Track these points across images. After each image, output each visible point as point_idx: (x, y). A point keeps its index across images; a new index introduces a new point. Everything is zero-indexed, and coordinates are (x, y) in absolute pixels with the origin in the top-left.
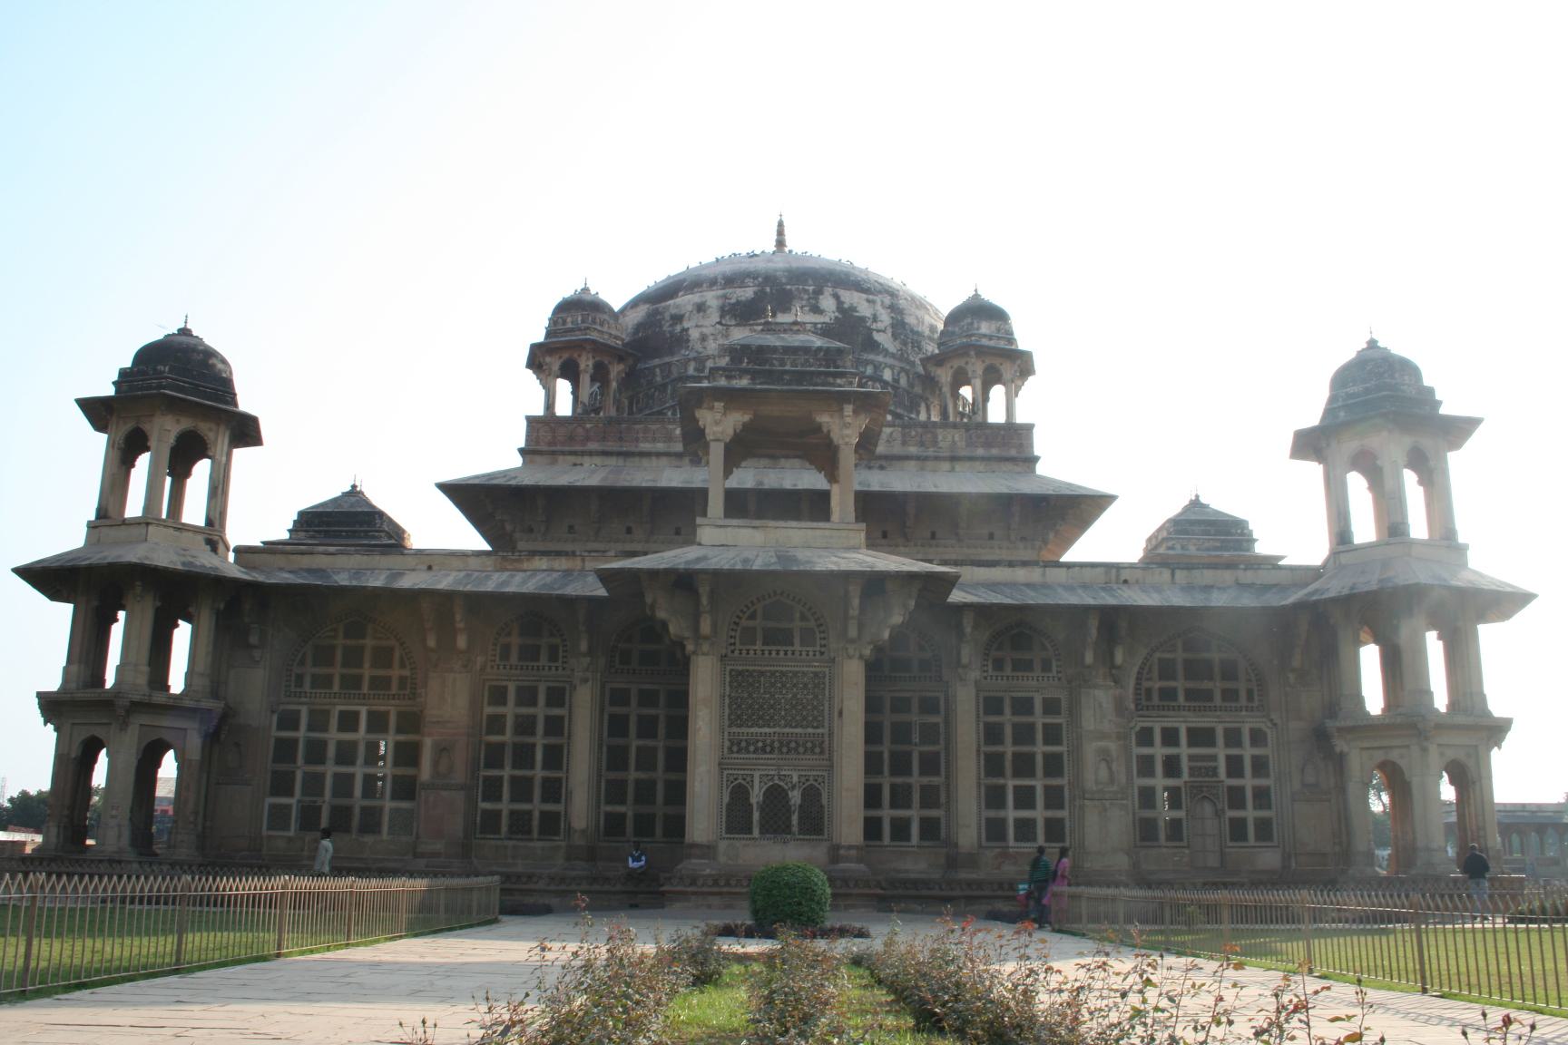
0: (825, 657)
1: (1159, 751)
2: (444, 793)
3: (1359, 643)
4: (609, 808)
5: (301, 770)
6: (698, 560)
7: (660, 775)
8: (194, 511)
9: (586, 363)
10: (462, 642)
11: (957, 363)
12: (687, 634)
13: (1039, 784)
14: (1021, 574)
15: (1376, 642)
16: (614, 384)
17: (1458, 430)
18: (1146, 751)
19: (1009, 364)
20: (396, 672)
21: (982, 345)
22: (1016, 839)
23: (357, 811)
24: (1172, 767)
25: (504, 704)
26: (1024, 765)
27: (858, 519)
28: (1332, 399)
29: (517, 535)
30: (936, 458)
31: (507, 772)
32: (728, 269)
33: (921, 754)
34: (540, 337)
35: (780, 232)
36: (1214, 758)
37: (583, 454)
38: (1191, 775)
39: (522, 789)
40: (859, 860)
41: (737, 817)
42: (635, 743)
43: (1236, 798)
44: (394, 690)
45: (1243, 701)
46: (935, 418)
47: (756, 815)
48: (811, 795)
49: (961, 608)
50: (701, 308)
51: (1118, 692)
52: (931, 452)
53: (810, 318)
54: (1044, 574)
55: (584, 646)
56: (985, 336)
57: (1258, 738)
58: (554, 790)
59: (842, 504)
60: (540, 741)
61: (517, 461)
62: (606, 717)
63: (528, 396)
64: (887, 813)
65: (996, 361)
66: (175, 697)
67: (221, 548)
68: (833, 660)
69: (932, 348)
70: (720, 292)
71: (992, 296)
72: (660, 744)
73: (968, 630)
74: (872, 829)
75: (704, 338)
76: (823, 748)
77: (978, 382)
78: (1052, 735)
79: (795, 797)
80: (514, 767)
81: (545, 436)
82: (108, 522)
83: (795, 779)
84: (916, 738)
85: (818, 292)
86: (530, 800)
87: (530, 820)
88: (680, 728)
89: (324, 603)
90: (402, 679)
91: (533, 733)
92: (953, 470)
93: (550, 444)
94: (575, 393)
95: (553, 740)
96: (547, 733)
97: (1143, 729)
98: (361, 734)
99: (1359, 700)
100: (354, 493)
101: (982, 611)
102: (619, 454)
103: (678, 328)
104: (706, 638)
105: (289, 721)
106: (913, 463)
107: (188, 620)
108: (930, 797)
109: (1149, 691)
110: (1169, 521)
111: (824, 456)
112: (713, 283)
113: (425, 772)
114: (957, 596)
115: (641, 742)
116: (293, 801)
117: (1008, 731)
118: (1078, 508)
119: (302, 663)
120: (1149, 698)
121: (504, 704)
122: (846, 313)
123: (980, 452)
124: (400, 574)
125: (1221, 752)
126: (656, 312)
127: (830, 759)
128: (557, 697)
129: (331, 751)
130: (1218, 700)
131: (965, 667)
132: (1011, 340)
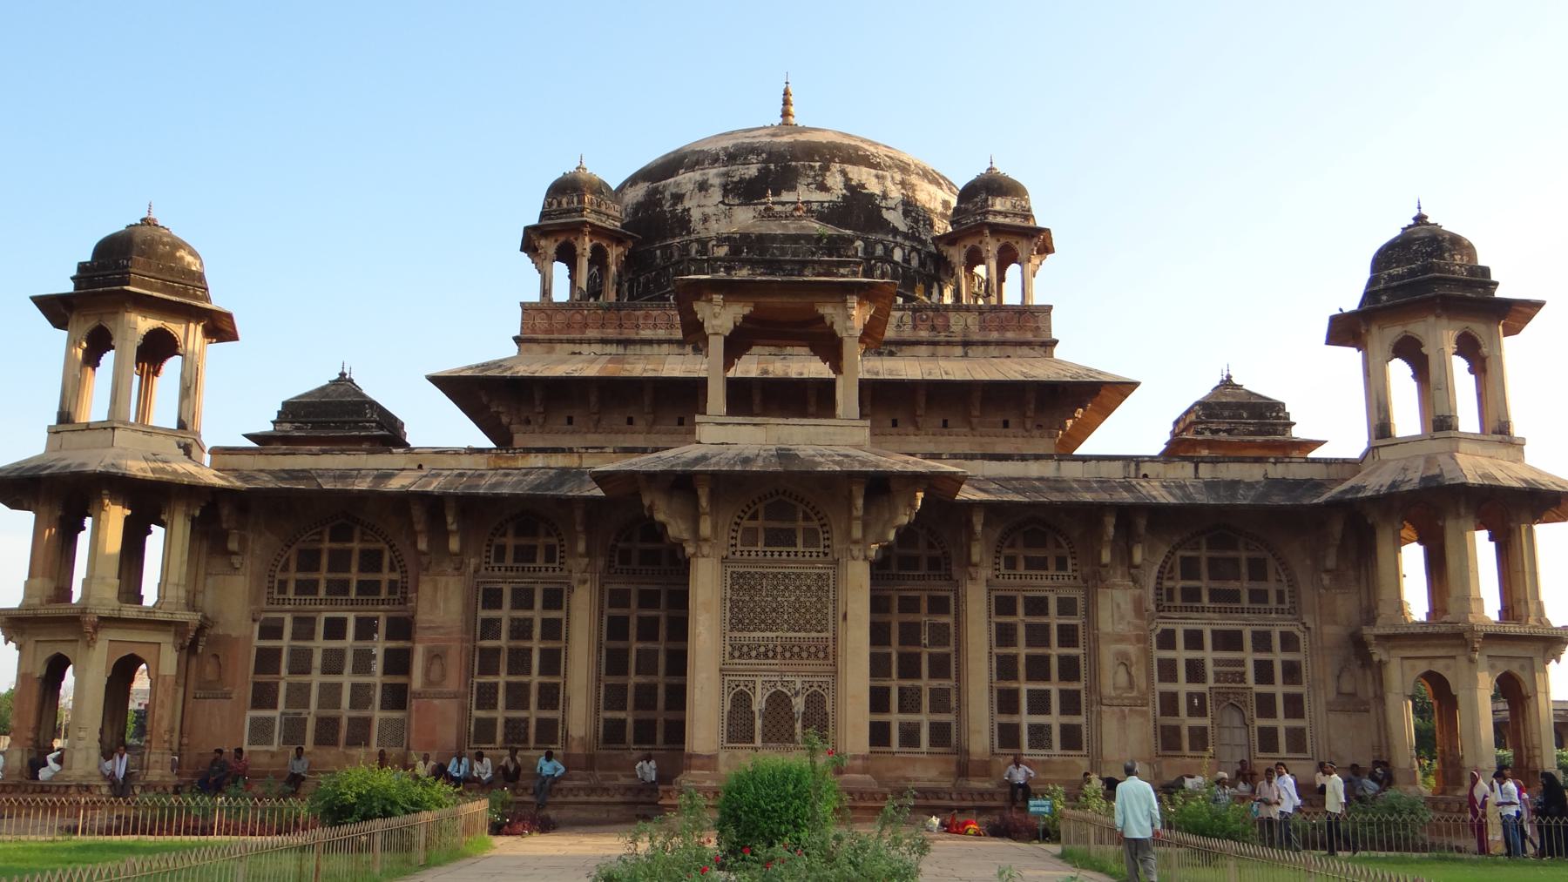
0: (829, 558)
1: (1181, 654)
2: (436, 702)
3: (1400, 542)
4: (609, 715)
5: (285, 680)
6: (697, 460)
7: (661, 679)
8: (164, 413)
9: (585, 245)
10: (454, 544)
11: (969, 243)
12: (685, 536)
13: (1054, 687)
14: (1034, 469)
15: (1420, 542)
16: (613, 268)
17: (1518, 313)
18: (1169, 687)
19: (1029, 240)
20: (386, 576)
21: (995, 221)
22: (1031, 747)
23: (344, 722)
24: (1195, 671)
25: (499, 607)
26: (1038, 668)
27: (862, 416)
28: (1372, 282)
29: (513, 427)
30: (948, 343)
31: (502, 679)
32: (729, 143)
33: (930, 655)
34: (534, 220)
35: (786, 102)
36: (1241, 663)
37: (581, 342)
38: (1217, 681)
39: (518, 695)
40: (865, 771)
41: (738, 728)
42: (635, 646)
43: (1266, 705)
44: (384, 594)
45: (1273, 602)
46: (948, 299)
47: (758, 723)
48: (815, 702)
49: (971, 505)
50: (703, 186)
51: (1137, 592)
52: (942, 337)
53: (819, 196)
54: (1058, 469)
55: (581, 547)
56: (1000, 213)
57: (1289, 642)
58: (550, 696)
59: (847, 398)
60: (536, 645)
61: (512, 350)
62: (605, 619)
63: (522, 281)
64: (895, 718)
65: (1012, 241)
66: (149, 611)
67: (195, 451)
68: (837, 562)
69: (942, 227)
70: (723, 169)
71: (1008, 168)
72: (661, 646)
73: (978, 528)
74: (879, 734)
75: (705, 219)
76: (828, 653)
77: (993, 265)
78: (1068, 636)
79: (799, 704)
80: (510, 673)
81: (540, 324)
82: (69, 427)
83: (799, 686)
84: (925, 639)
85: (825, 168)
86: (527, 707)
87: (527, 727)
88: (680, 629)
89: (318, 504)
90: (393, 584)
91: (530, 638)
92: (966, 355)
93: (546, 332)
94: (572, 277)
95: (550, 644)
96: (544, 637)
97: (1164, 631)
98: (349, 642)
99: (1399, 606)
100: (343, 380)
101: (993, 510)
102: (619, 342)
103: (679, 208)
104: (706, 540)
105: (271, 630)
106: (924, 348)
107: (161, 524)
108: (940, 701)
109: (1170, 591)
110: (1198, 403)
111: (830, 348)
112: (715, 160)
113: (417, 681)
114: (966, 494)
115: (641, 645)
116: (275, 714)
117: (1021, 632)
118: (1099, 395)
119: (285, 569)
120: (1171, 597)
121: (499, 607)
122: (855, 192)
123: (994, 336)
124: (387, 475)
125: (1249, 656)
126: (656, 191)
127: (835, 664)
128: (554, 599)
129: (317, 660)
130: (1245, 602)
131: (975, 565)
132: (1027, 215)
